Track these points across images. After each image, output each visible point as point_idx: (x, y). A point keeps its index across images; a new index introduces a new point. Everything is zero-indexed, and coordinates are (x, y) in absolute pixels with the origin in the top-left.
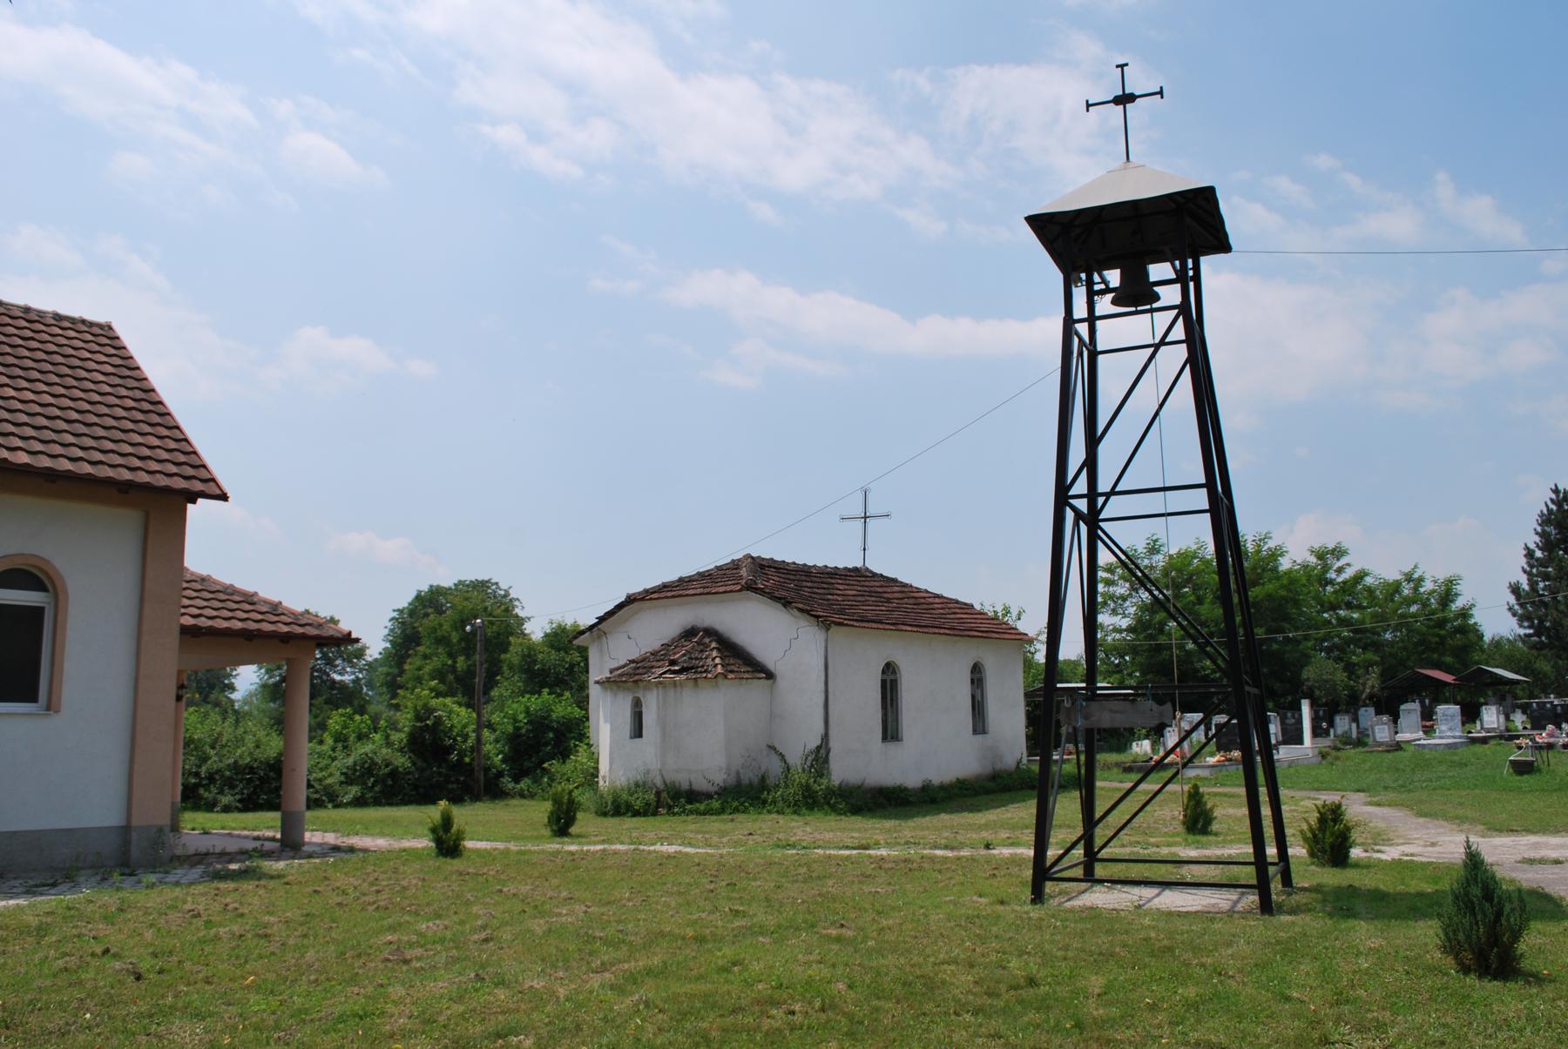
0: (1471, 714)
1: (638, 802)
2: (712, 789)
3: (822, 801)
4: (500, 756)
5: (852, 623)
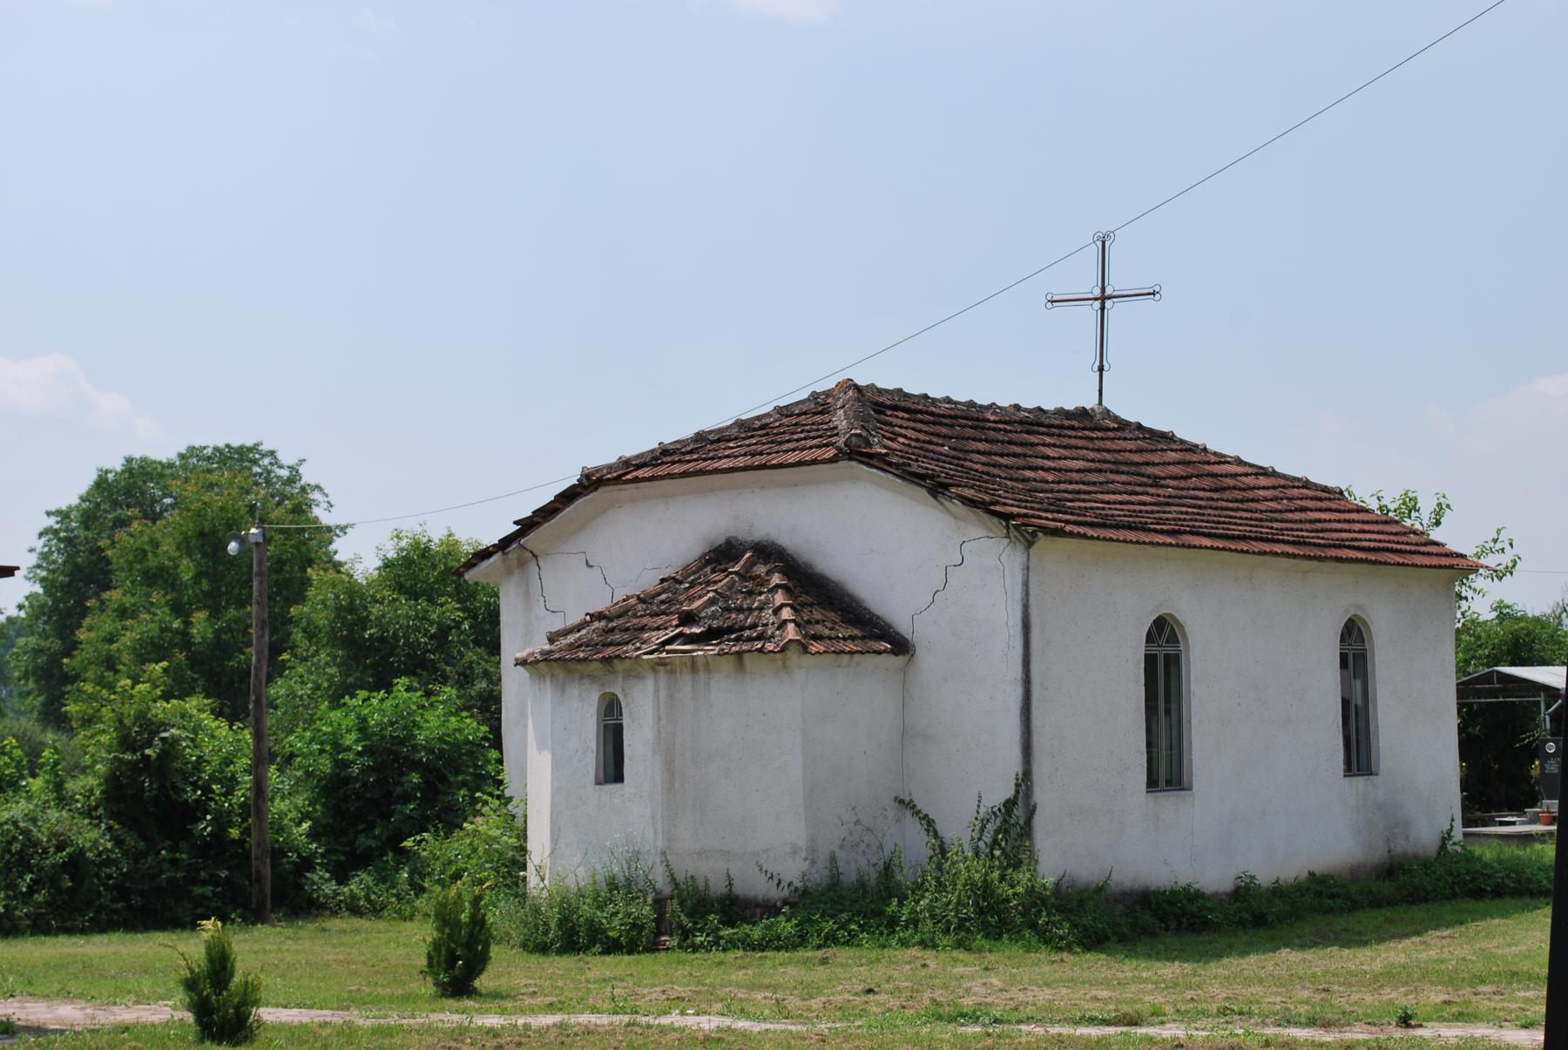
1: (616, 922)
2: (777, 894)
3: (1019, 920)
4: (305, 826)
5: (1082, 530)
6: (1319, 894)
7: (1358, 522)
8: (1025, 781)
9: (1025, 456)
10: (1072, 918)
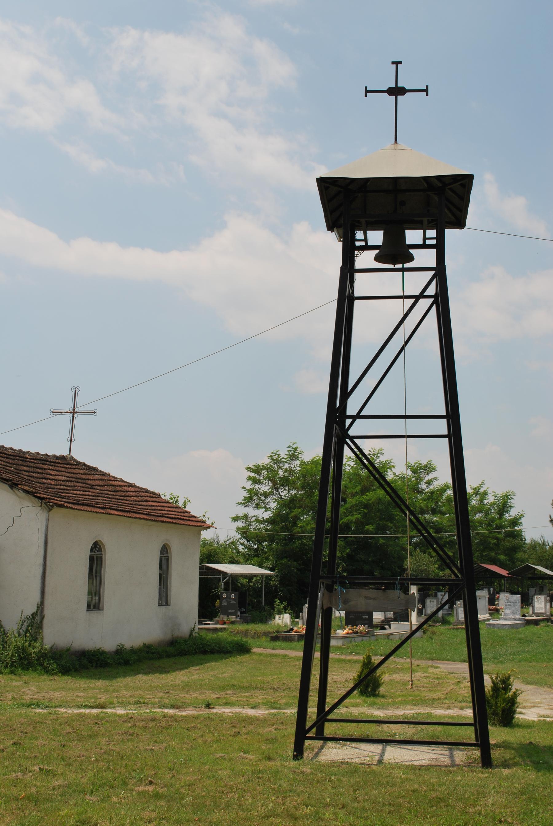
0: (526, 601)
3: (35, 662)
6: (148, 652)
7: (167, 507)
8: (41, 605)
9: (42, 473)
10: (57, 662)
